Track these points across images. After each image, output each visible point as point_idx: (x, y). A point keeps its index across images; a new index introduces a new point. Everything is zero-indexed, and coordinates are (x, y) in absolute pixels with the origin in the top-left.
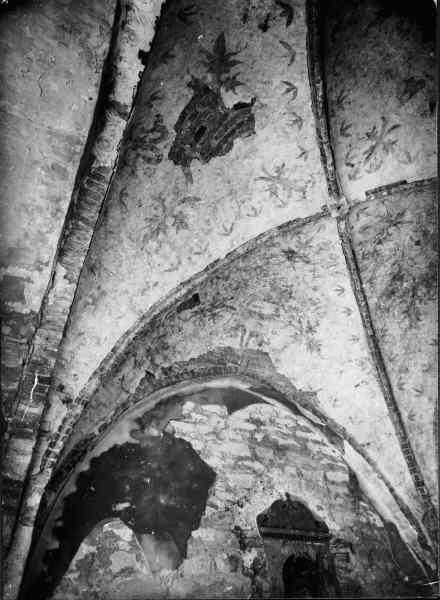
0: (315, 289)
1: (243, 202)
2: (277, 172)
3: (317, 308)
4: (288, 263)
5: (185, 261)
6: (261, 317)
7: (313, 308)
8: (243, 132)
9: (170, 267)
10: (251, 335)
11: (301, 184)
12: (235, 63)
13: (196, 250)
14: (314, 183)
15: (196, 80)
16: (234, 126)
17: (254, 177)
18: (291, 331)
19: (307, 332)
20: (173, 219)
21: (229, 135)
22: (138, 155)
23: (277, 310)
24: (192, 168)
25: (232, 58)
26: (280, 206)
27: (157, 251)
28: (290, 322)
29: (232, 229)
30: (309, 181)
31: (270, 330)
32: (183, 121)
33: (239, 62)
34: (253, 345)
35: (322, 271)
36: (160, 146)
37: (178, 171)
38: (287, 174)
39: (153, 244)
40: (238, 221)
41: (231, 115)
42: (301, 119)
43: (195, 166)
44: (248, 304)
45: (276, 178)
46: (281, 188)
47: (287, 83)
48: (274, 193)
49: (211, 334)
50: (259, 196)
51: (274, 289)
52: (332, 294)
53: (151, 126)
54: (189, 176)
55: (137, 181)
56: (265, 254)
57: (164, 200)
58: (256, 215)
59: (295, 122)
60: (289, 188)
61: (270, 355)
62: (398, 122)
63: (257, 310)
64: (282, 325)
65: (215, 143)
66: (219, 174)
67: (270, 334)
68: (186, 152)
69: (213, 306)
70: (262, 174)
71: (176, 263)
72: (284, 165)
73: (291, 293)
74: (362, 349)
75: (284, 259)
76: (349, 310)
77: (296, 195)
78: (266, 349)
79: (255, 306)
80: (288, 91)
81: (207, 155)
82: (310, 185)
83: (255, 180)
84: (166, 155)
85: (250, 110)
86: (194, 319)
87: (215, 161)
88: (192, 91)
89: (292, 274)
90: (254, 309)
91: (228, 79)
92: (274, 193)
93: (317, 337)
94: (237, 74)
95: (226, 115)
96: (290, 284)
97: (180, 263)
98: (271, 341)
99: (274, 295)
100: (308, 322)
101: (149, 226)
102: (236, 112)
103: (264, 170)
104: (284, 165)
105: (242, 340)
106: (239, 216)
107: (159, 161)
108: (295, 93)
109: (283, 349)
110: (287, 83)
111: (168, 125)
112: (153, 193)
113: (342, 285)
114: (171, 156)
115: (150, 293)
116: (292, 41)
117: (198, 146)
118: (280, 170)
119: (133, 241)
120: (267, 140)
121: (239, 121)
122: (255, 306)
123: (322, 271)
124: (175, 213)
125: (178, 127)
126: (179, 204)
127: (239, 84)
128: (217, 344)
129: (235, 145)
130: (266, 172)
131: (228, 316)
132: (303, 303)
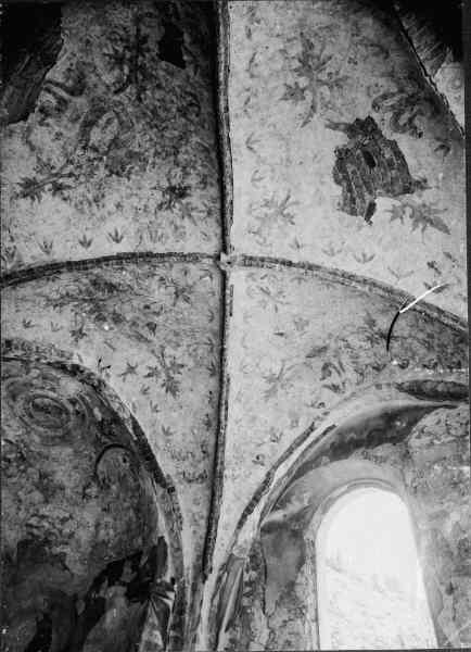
0: (119, 206)
1: (273, 171)
2: (289, 214)
3: (90, 204)
4: (165, 184)
5: (250, 82)
6: (88, 125)
7: (90, 196)
8: (345, 199)
9: (256, 61)
10: (61, 101)
11: (265, 232)
12: (415, 226)
13: (253, 100)
14: (261, 244)
15: (422, 188)
16: (355, 195)
17: (293, 190)
18: (58, 161)
19: (54, 183)
20: (301, 86)
21: (349, 185)
22: (401, 91)
23: (95, 150)
24: (341, 133)
25: (421, 226)
26: (251, 206)
27: (283, 51)
28: (71, 162)
29: (251, 149)
30: (265, 239)
31: (65, 132)
32: (395, 153)
33: (414, 229)
34: (46, 99)
35: (145, 220)
36: (389, 116)
37: (348, 119)
38: (282, 223)
39: (297, 49)
40: (255, 158)
41: (368, 197)
42: (333, 255)
43: (341, 139)
44: (117, 114)
45: (282, 211)
46: (269, 212)
47: (372, 258)
48: (267, 204)
49: (88, 42)
50: (272, 189)
51: (131, 155)
52: (109, 227)
53: (416, 122)
54: (335, 126)
55: (376, 73)
56: (195, 168)
57: (331, 88)
58: (253, 180)
59: (332, 250)
60: (264, 219)
61: (21, 123)
62: (280, 312)
63: (102, 122)
64: (70, 149)
65: (350, 168)
66: (316, 157)
67: (57, 129)
68: (360, 136)
69: (135, 68)
70: (290, 200)
71: (255, 71)
72: (293, 223)
73: (118, 174)
74: (33, 257)
75: (174, 182)
76: (89, 244)
77: (257, 224)
78: (34, 117)
79: (109, 122)
80: (364, 255)
81: (343, 156)
82: (261, 240)
83: (289, 191)
84: (375, 116)
85: (362, 215)
86: (133, 32)
87: (331, 160)
88: (416, 178)
89: (147, 184)
90: (105, 118)
91: (404, 212)
92: (267, 204)
93: (46, 196)
94: (402, 222)
95: (371, 193)
96: (133, 177)
97: (252, 76)
98: (44, 128)
99: (122, 153)
100: (69, 187)
101: (318, 58)
102: (368, 202)
103: (297, 203)
104: (293, 223)
105: (57, 84)
106: (261, 161)
107: (375, 106)
108: (359, 261)
109: (28, 143)
110: (372, 258)
111: (402, 135)
112: (349, 81)
113: (124, 240)
114: (370, 120)
115: (245, 22)
116: (410, 280)
117: (359, 151)
118: (290, 218)
119: (320, 28)
120: (326, 218)
121: (358, 201)
122: (109, 122)
123: (145, 220)
124: (307, 92)
125: (393, 145)
126: (313, 101)
127: (393, 219)
128: (65, 46)
129: (334, 186)
130: (290, 205)
131: (109, 78)
132: (100, 186)
